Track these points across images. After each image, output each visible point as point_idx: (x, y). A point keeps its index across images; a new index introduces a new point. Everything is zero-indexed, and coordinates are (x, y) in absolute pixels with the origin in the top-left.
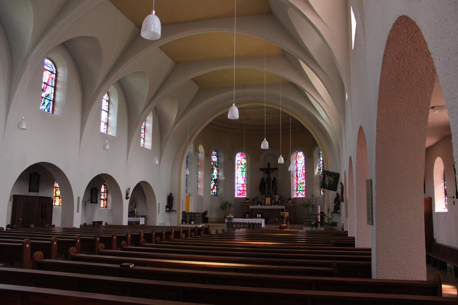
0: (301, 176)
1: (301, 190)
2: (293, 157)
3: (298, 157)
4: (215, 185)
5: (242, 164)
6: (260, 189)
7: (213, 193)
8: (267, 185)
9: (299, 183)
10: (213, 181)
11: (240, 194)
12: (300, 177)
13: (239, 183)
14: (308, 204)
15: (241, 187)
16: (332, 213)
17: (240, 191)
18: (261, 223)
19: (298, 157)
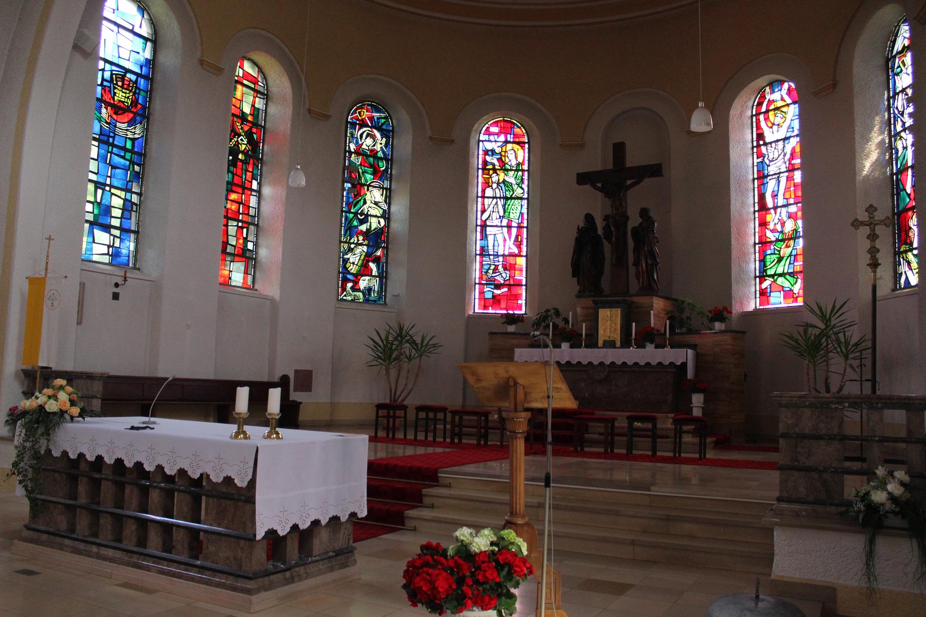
0: (781, 201)
1: (780, 275)
2: (741, 114)
3: (767, 111)
4: (369, 257)
5: (508, 167)
6: (576, 270)
7: (360, 295)
8: (607, 247)
9: (771, 236)
10: (361, 238)
11: (496, 300)
12: (775, 208)
14: (823, 333)
18: (252, 483)
19: (767, 111)
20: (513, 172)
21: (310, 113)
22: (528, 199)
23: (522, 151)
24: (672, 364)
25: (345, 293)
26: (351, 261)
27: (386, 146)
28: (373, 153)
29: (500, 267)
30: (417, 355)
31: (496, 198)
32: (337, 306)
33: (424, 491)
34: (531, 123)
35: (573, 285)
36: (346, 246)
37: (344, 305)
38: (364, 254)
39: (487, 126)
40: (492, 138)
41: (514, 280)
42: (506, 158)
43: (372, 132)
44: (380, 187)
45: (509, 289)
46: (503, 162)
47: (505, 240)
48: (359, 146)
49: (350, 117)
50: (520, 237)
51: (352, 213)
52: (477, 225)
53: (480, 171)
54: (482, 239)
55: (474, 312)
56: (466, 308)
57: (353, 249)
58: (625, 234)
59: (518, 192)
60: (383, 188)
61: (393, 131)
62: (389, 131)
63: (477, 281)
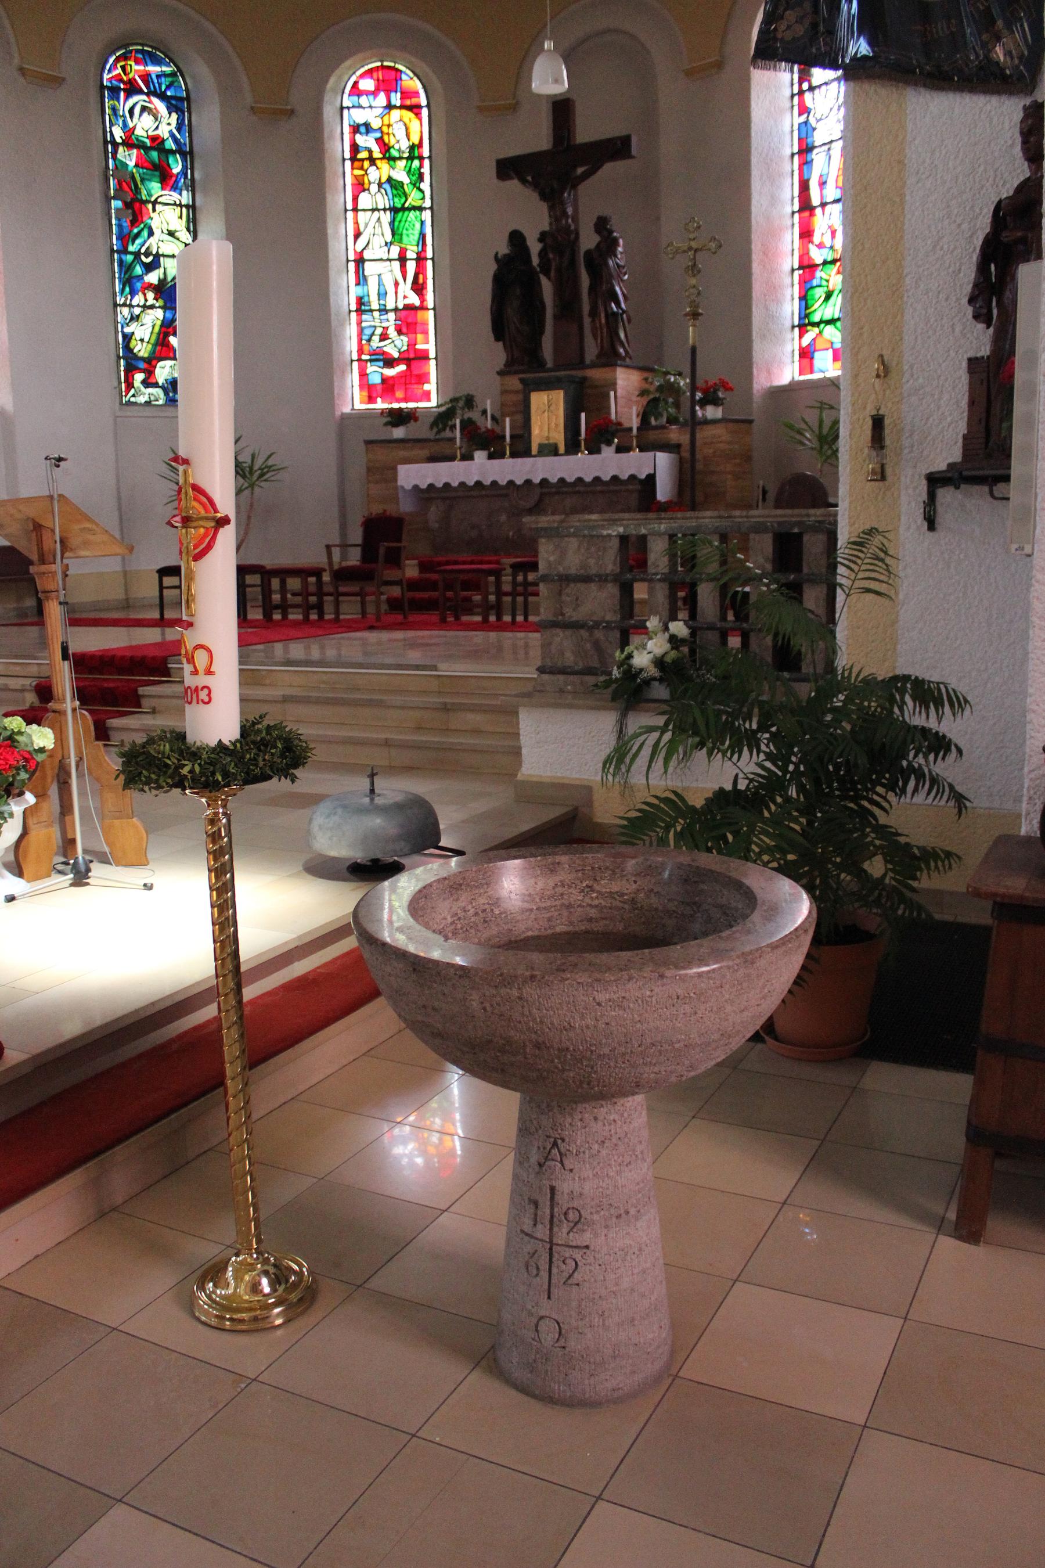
5: (394, 153)
6: (499, 330)
7: (158, 392)
8: (547, 287)
9: (817, 256)
10: (150, 295)
11: (388, 386)
12: (823, 205)
13: (375, 305)
15: (392, 332)
16: (935, 481)
17: (390, 362)
20: (404, 161)
21: (24, 75)
22: (431, 208)
23: (418, 122)
24: (633, 477)
25: (132, 391)
26: (138, 336)
27: (179, 128)
28: (157, 142)
29: (392, 332)
30: (246, 485)
31: (378, 210)
32: (119, 414)
33: (141, 690)
34: (428, 70)
35: (499, 355)
36: (125, 311)
37: (130, 411)
38: (159, 323)
39: (353, 79)
40: (364, 100)
41: (416, 351)
42: (391, 136)
43: (150, 102)
44: (175, 204)
45: (409, 366)
46: (385, 144)
47: (397, 284)
48: (129, 132)
49: (106, 76)
50: (421, 276)
51: (131, 253)
52: (348, 261)
53: (348, 164)
54: (358, 284)
55: (353, 409)
56: (337, 401)
57: (138, 316)
58: (573, 263)
59: (414, 198)
60: (181, 206)
61: (188, 98)
62: (180, 99)
63: (355, 357)
